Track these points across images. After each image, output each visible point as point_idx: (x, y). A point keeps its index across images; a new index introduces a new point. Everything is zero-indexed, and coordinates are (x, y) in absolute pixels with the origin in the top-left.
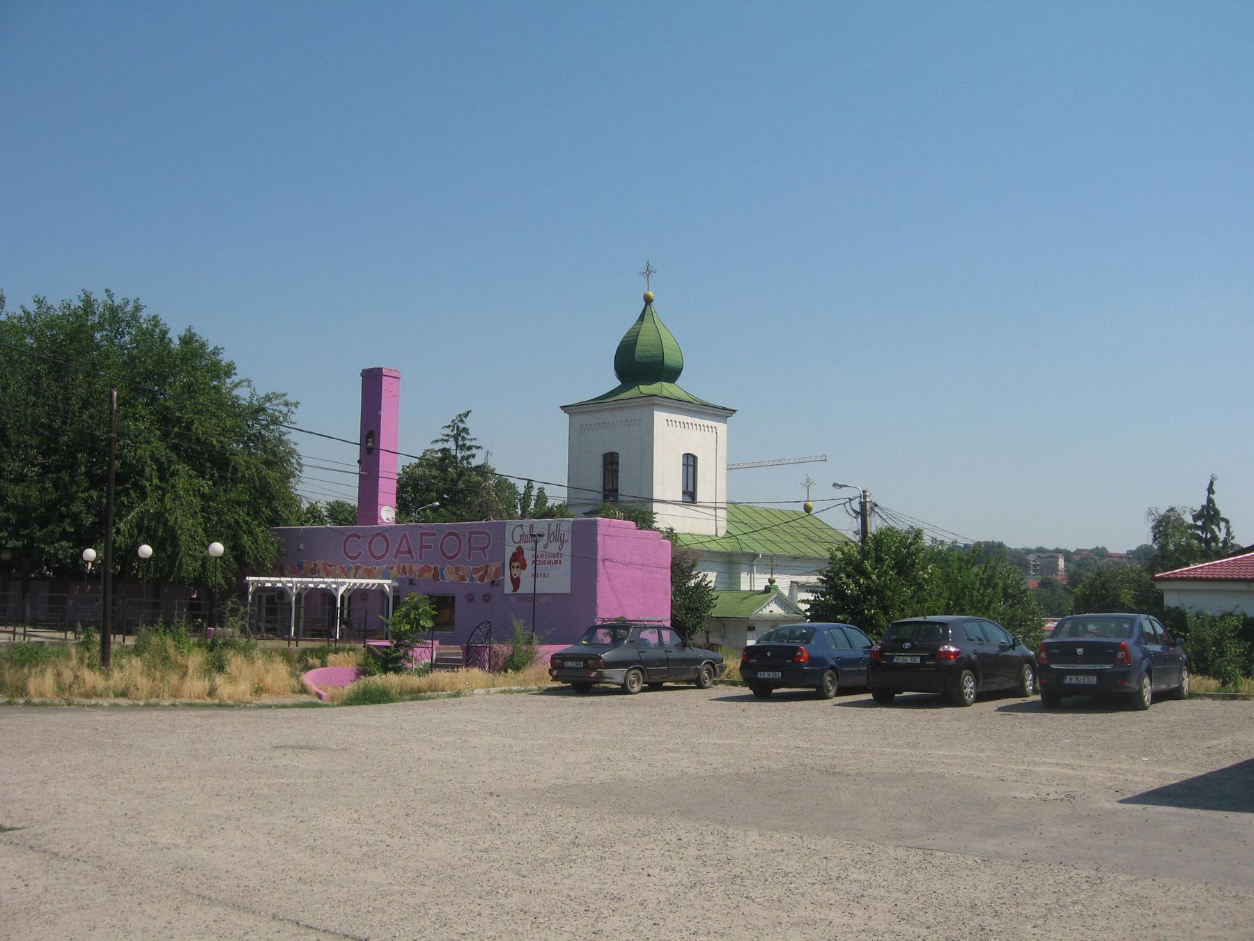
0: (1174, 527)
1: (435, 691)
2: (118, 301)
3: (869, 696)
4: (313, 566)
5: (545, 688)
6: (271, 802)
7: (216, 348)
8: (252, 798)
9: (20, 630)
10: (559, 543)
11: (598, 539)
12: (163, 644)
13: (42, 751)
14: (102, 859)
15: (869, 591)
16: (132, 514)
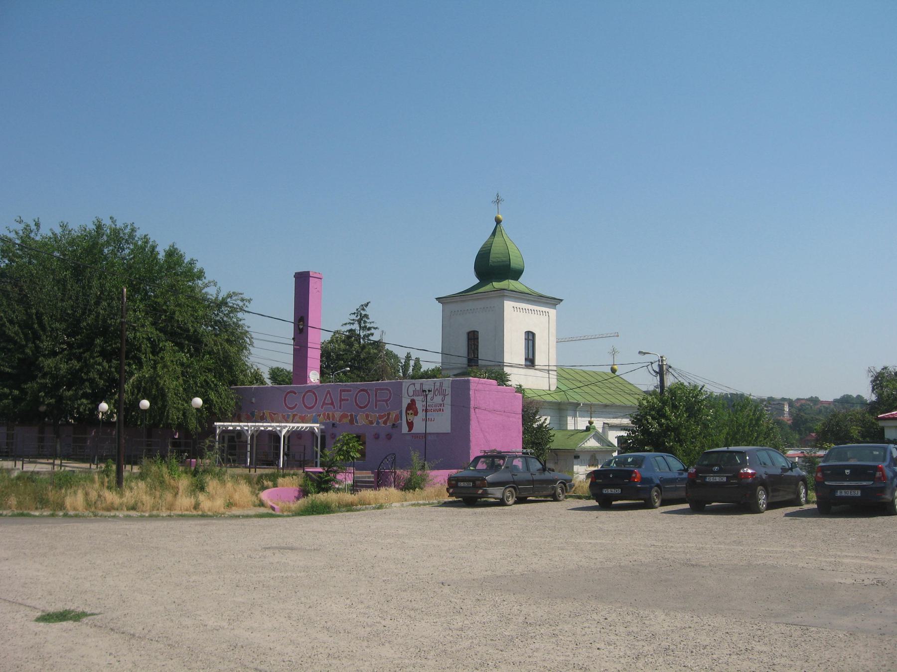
0: (888, 381)
1: (364, 504)
2: (119, 225)
3: (687, 506)
4: (262, 414)
5: (443, 502)
6: (280, 592)
7: (192, 260)
8: (264, 588)
9: (58, 462)
10: (442, 396)
11: (471, 393)
12: (161, 471)
13: (94, 552)
14: (170, 639)
15: (668, 428)
16: (133, 378)
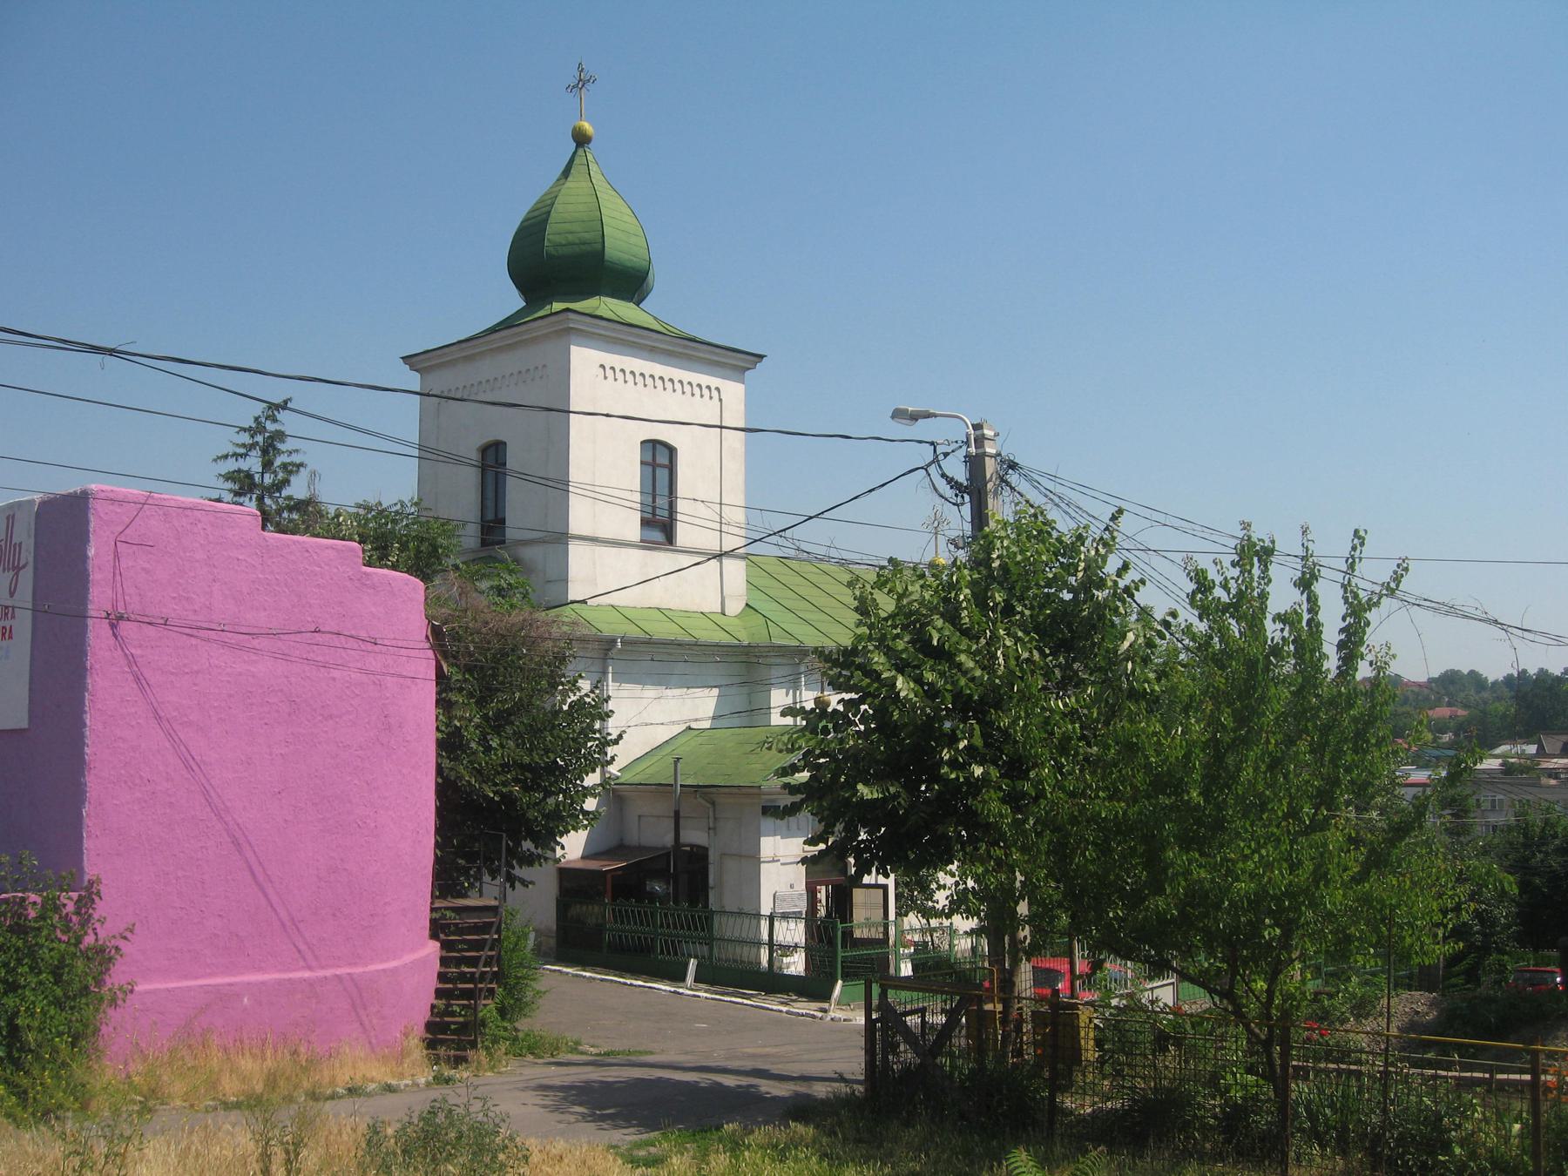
11: (91, 552)
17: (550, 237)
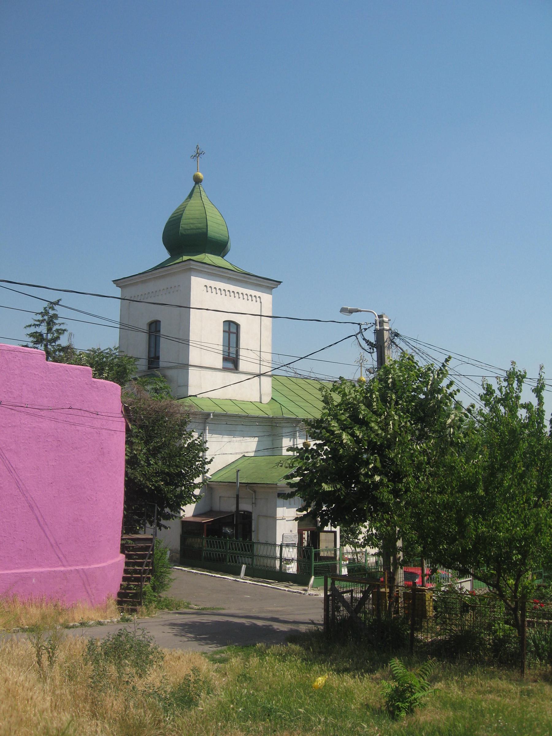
17: (183, 226)
